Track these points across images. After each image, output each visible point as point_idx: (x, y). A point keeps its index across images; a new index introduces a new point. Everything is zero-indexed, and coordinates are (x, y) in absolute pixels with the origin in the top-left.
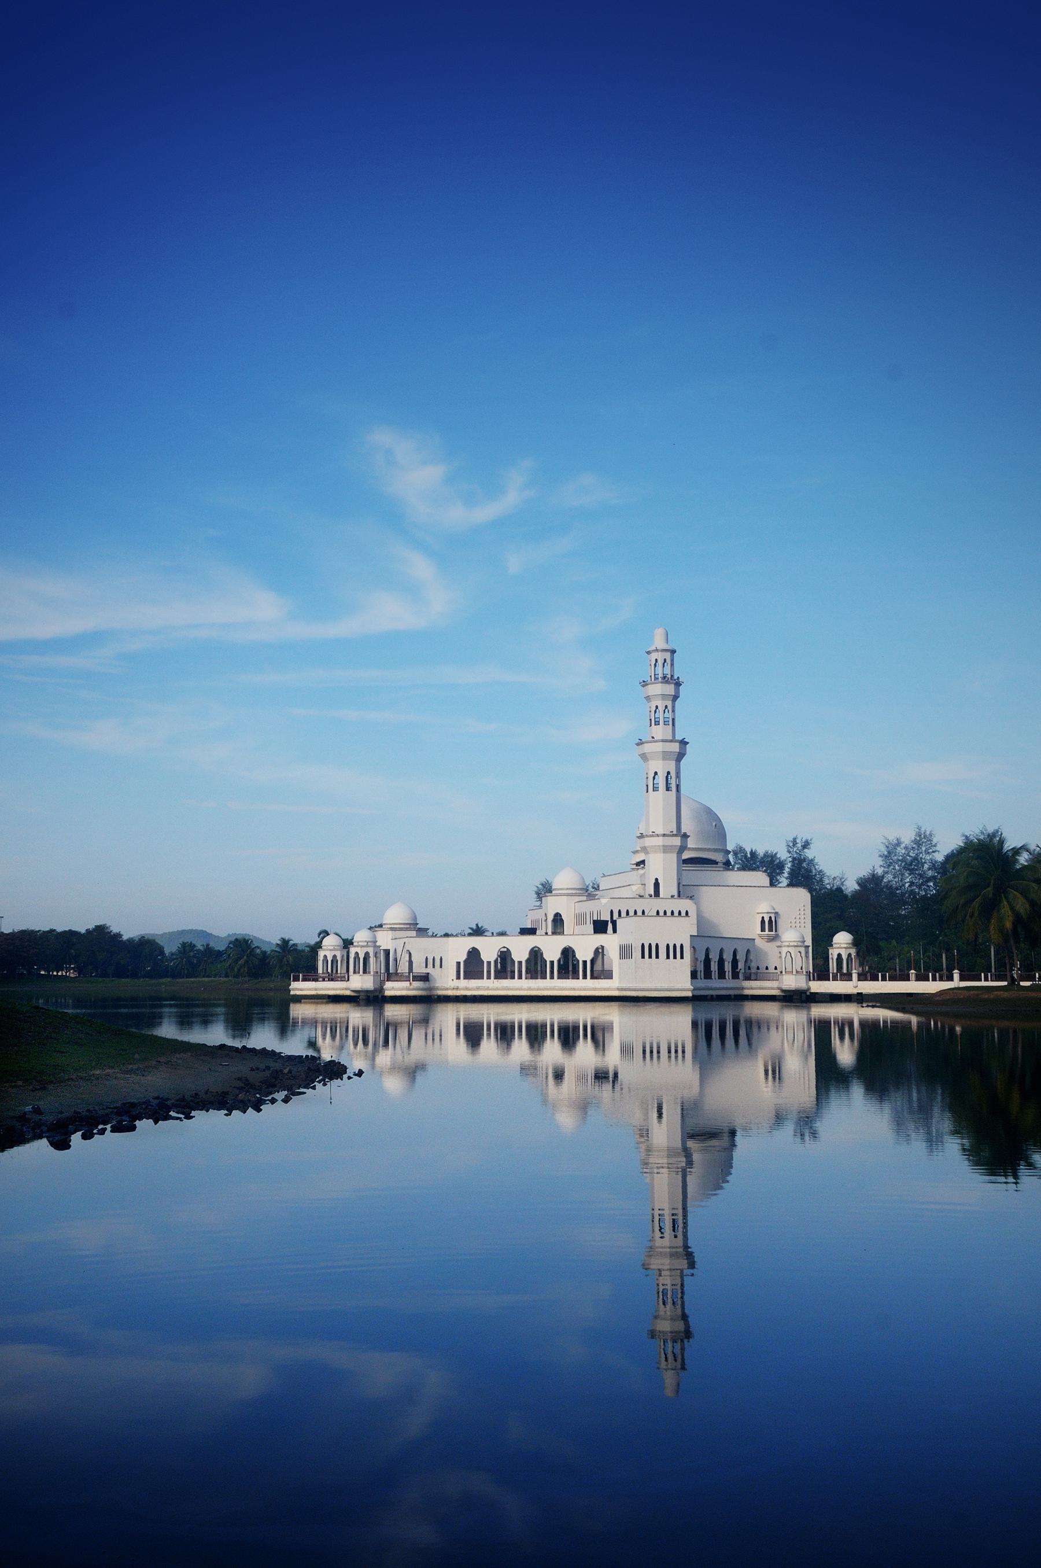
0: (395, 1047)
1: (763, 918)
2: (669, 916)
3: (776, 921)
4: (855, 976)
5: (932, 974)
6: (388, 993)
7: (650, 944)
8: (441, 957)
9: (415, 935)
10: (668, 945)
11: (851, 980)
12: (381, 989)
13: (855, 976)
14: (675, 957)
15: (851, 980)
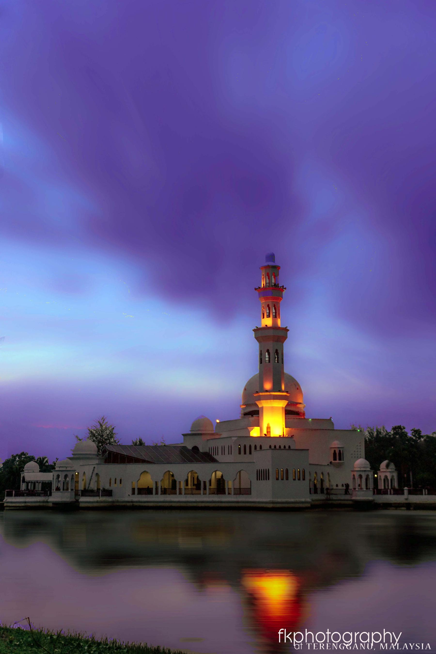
0: (126, 642)
1: (335, 451)
2: (278, 449)
3: (343, 453)
4: (406, 492)
5: (20, 490)
6: (82, 505)
7: (266, 469)
8: (111, 478)
9: (259, 428)
10: (257, 470)
11: (403, 494)
12: (77, 501)
13: (406, 492)
14: (259, 480)
15: (403, 494)
